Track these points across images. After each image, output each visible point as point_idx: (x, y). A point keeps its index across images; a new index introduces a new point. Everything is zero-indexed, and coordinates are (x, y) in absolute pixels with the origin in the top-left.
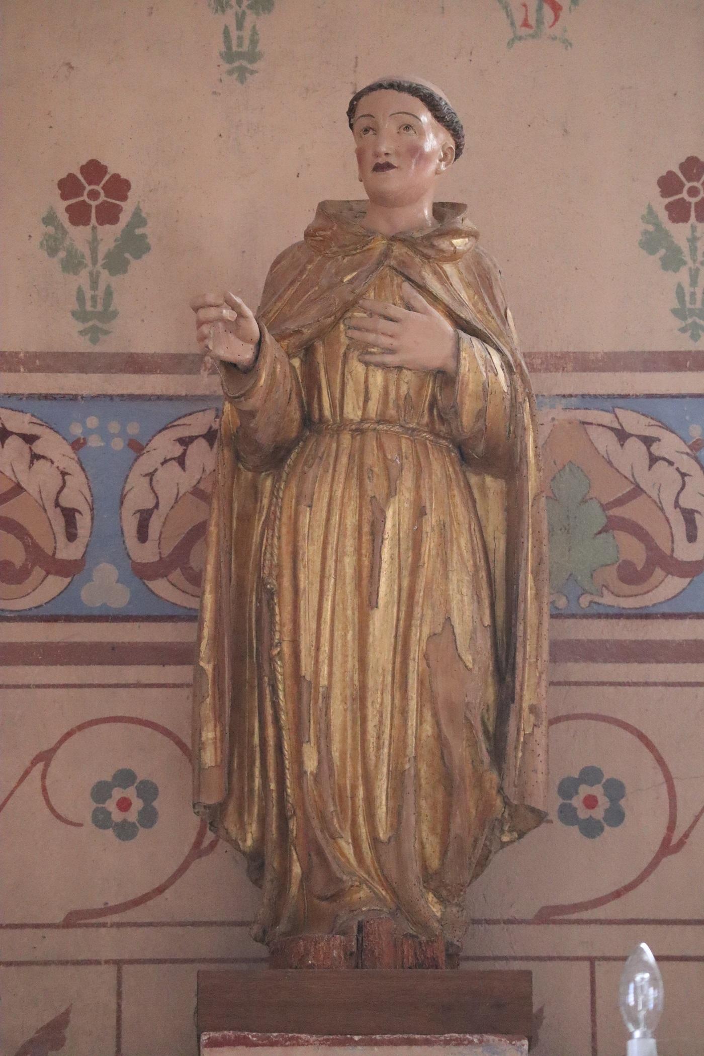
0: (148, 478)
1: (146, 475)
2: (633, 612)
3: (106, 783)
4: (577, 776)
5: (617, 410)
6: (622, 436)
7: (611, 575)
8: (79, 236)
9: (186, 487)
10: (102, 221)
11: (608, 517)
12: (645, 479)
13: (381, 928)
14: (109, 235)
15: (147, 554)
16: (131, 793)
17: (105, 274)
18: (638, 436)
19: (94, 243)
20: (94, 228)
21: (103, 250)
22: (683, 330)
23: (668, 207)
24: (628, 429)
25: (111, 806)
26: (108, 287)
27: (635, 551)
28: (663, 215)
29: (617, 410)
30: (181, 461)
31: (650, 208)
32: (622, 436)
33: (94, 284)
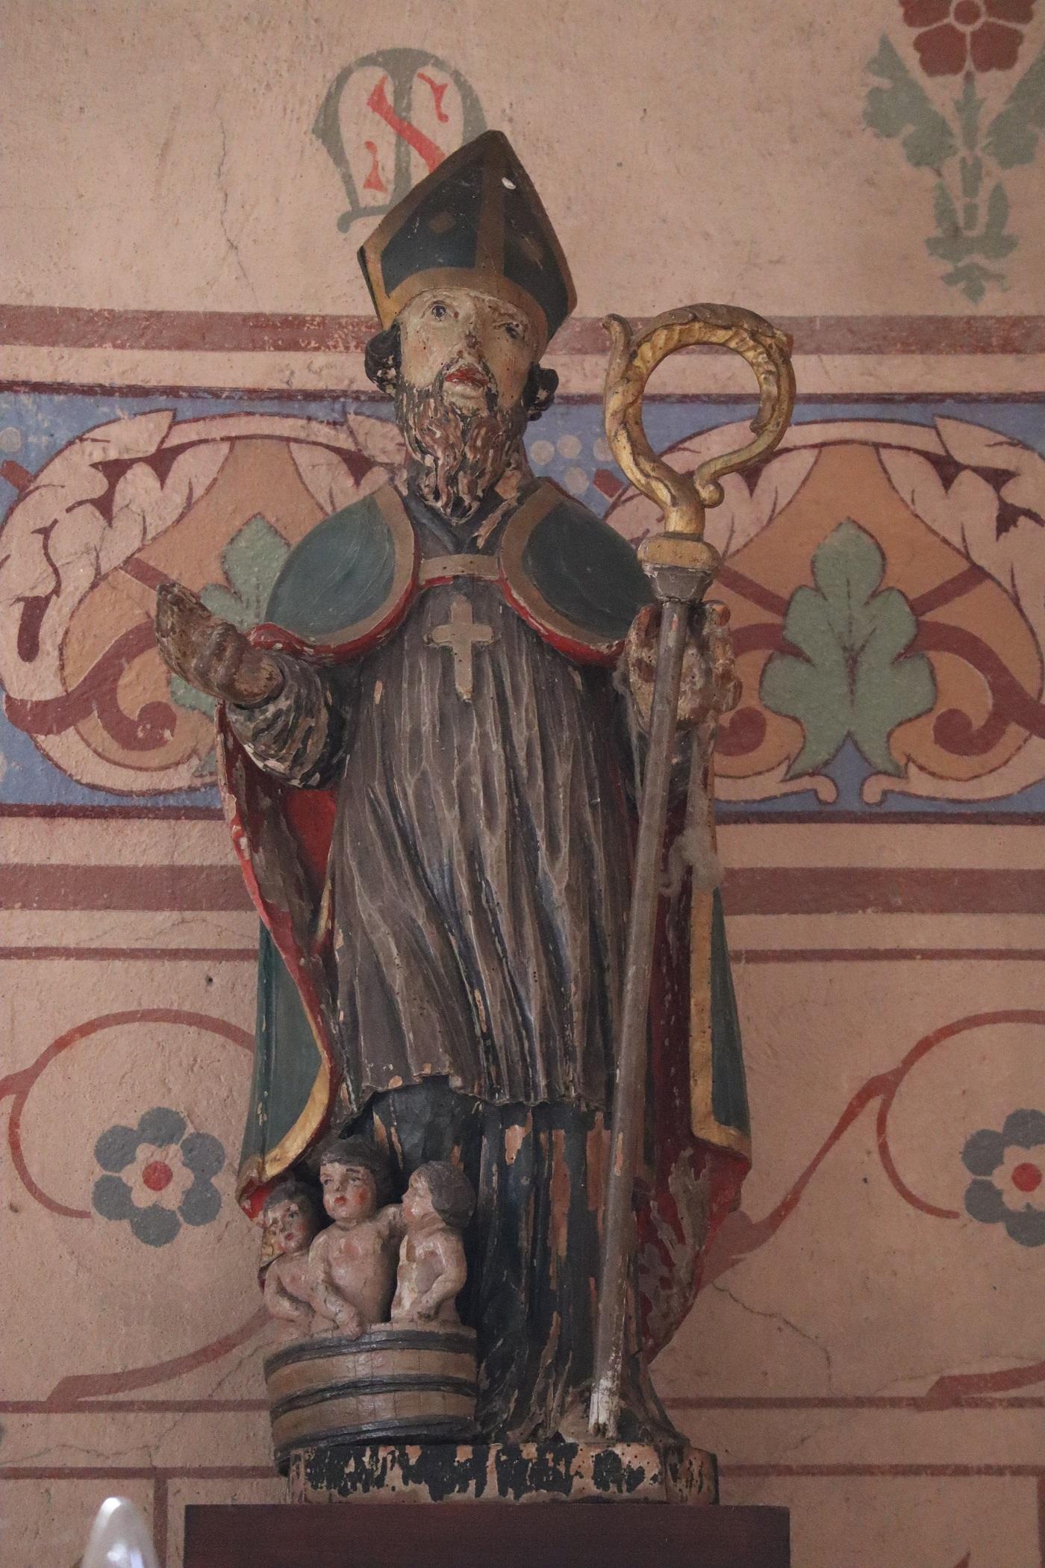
0: (41, 537)
1: (39, 531)
2: (740, 808)
3: (126, 1131)
4: (1000, 1129)
5: (941, 423)
6: (946, 468)
7: (920, 739)
8: (942, 92)
9: (114, 555)
10: (984, 65)
11: (919, 625)
12: (987, 552)
13: (541, 1432)
14: (995, 88)
15: (39, 683)
16: (173, 1155)
17: (991, 163)
18: (976, 470)
19: (968, 105)
20: (969, 78)
21: (985, 119)
22: (950, 279)
23: (920, 44)
24: (959, 457)
25: (132, 1175)
26: (998, 188)
27: (969, 693)
28: (911, 59)
29: (941, 423)
30: (104, 505)
31: (885, 44)
32: (946, 468)
33: (971, 183)
